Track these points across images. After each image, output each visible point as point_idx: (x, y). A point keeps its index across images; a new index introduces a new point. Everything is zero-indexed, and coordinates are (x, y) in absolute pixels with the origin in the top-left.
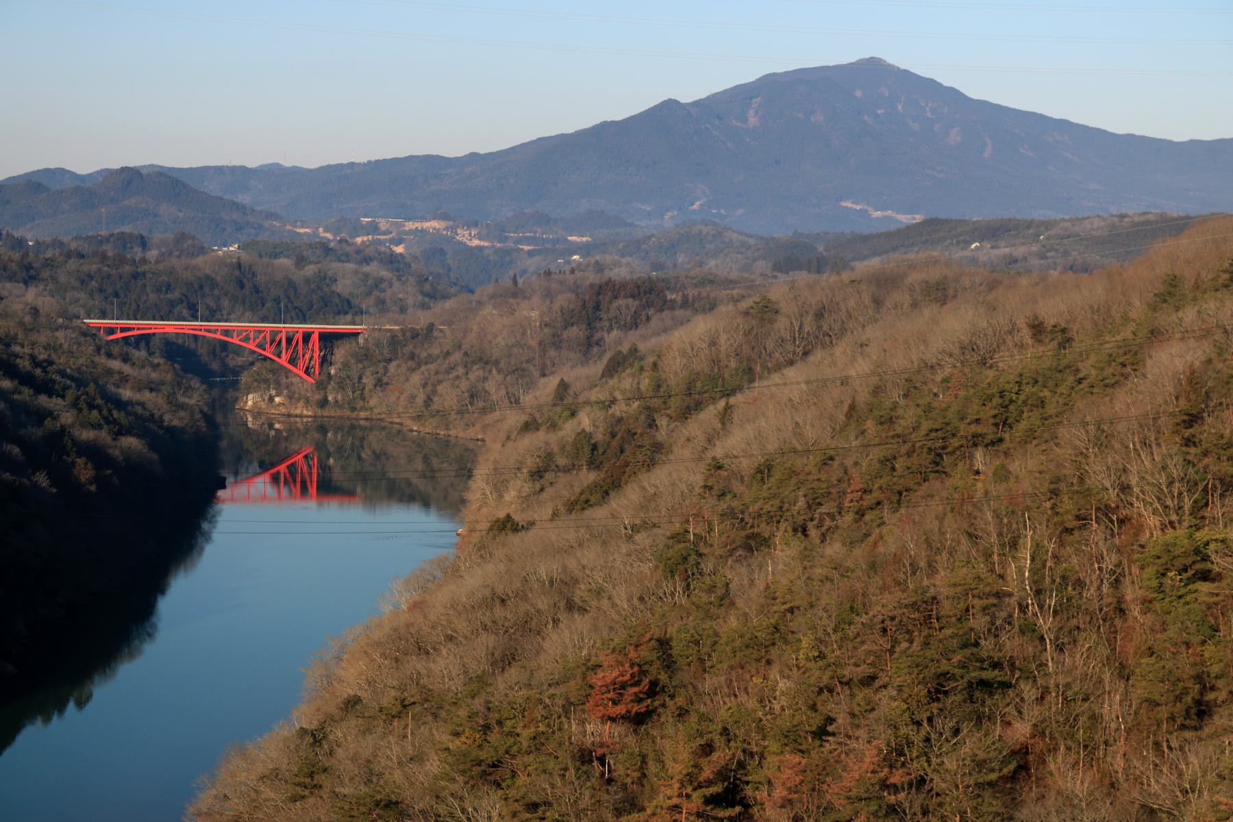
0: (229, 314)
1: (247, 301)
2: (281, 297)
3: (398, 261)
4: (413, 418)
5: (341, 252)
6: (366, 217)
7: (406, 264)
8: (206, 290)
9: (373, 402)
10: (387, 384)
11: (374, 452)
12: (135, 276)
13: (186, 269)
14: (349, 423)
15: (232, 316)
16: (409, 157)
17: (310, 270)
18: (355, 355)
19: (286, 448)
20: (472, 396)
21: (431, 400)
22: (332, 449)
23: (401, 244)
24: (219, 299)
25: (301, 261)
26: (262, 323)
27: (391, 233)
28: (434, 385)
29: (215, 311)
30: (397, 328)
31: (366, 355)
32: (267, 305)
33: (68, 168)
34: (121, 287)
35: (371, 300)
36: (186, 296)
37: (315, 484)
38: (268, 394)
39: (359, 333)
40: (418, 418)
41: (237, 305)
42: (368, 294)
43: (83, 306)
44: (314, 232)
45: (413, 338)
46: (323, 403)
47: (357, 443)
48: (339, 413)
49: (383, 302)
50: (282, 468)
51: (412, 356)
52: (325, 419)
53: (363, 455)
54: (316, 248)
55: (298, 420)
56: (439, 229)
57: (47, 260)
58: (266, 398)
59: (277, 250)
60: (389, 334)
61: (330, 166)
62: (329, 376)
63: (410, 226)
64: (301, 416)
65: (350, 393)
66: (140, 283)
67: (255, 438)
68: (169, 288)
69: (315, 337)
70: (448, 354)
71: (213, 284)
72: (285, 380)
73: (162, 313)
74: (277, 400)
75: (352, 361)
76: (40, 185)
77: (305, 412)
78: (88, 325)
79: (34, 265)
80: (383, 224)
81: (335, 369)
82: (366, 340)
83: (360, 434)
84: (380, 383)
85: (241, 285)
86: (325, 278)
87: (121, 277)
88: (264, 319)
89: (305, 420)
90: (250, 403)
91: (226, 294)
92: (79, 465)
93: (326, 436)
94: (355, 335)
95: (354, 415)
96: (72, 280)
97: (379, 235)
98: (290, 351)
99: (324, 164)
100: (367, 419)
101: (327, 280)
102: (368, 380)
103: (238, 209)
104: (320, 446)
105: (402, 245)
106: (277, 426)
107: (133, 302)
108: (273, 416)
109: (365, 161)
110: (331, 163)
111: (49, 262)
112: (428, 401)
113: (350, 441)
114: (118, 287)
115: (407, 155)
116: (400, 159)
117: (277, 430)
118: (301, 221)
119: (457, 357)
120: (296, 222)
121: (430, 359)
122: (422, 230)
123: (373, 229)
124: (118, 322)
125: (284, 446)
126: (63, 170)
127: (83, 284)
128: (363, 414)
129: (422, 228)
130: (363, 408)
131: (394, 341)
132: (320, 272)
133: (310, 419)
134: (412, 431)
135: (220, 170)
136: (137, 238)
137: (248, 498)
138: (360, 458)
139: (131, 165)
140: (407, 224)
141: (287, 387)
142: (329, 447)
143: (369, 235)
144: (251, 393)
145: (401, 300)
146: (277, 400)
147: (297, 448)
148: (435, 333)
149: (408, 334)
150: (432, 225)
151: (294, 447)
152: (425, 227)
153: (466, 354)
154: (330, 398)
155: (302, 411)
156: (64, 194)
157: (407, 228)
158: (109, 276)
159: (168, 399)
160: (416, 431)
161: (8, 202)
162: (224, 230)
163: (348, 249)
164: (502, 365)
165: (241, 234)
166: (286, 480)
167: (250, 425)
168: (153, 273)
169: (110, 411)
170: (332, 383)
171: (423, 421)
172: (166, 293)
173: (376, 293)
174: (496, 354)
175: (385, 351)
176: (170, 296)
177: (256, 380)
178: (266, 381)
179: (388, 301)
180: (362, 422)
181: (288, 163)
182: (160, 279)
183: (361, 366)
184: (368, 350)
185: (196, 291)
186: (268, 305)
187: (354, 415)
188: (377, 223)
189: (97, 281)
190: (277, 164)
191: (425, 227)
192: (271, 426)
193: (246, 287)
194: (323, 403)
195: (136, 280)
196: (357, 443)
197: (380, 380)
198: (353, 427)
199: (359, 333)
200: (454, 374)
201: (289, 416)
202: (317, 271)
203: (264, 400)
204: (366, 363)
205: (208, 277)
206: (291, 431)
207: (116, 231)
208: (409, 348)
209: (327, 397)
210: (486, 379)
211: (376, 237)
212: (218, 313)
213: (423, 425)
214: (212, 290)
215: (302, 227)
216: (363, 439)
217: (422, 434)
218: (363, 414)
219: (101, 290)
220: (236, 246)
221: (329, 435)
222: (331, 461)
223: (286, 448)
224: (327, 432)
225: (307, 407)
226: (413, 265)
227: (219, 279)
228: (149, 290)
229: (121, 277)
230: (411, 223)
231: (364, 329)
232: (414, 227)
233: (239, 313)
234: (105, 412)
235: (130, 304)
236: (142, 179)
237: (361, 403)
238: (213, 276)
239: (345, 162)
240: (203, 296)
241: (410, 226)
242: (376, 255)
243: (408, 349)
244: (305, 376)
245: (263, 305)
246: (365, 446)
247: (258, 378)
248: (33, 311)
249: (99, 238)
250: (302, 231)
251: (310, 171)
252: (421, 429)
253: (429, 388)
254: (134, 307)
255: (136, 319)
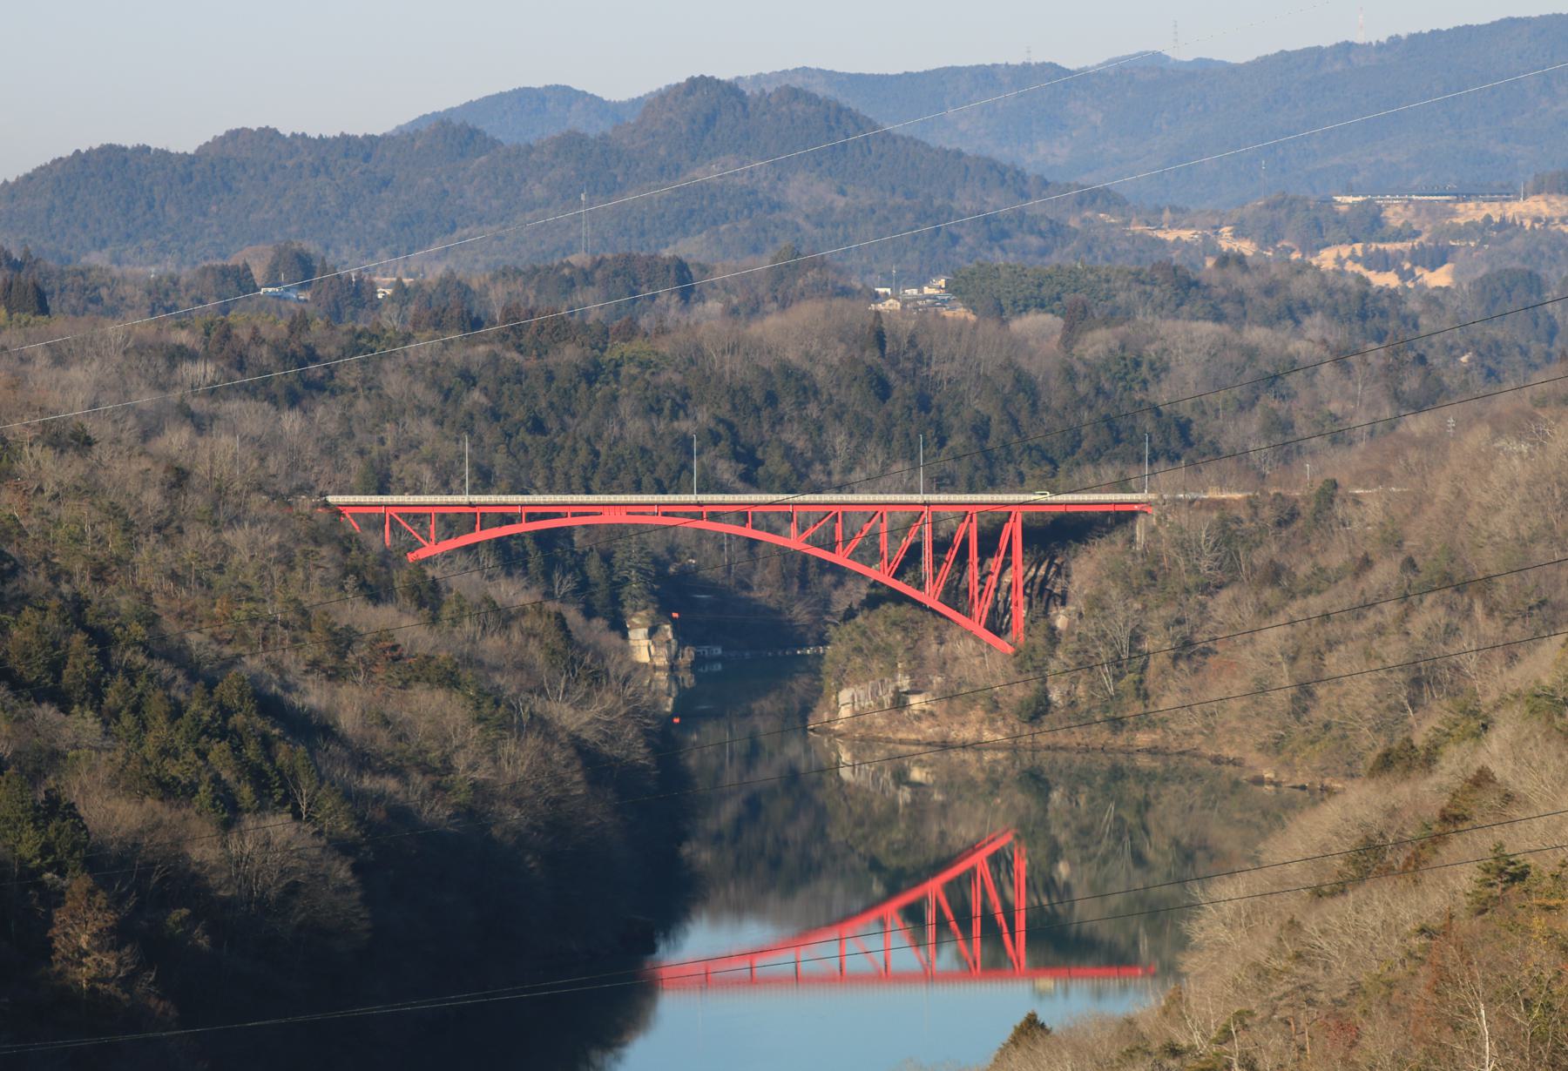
0: (848, 470)
1: (897, 431)
2: (993, 422)
3: (1383, 313)
4: (1262, 748)
5: (1222, 291)
6: (1350, 191)
7: (1404, 319)
8: (787, 405)
9: (1169, 701)
10: (1206, 652)
11: (1176, 842)
12: (591, 374)
13: (732, 350)
14: (1107, 764)
15: (858, 475)
16: (1502, 21)
17: (1097, 343)
18: (1121, 576)
19: (942, 835)
20: (1416, 682)
21: (1311, 695)
22: (1063, 837)
23: (1443, 262)
24: (820, 429)
25: (1078, 319)
26: (939, 491)
27: (1417, 234)
28: (1319, 654)
29: (808, 465)
30: (1237, 496)
31: (1151, 575)
32: (950, 443)
33: (578, 86)
34: (551, 405)
35: (1253, 423)
36: (730, 426)
37: (1021, 937)
38: (891, 688)
39: (1134, 514)
40: (1276, 746)
41: (870, 446)
42: (1244, 407)
43: (430, 461)
44: (1205, 237)
45: (1281, 524)
46: (1038, 710)
47: (1130, 818)
48: (1079, 737)
49: (1286, 426)
50: (933, 889)
51: (1275, 574)
52: (1043, 754)
53: (1150, 854)
54: (1153, 282)
55: (969, 756)
56: (1549, 220)
57: (359, 336)
58: (887, 699)
59: (1045, 291)
60: (1215, 515)
61: (1284, 56)
62: (1053, 636)
63: (1471, 212)
64: (977, 746)
65: (1107, 681)
66: (601, 391)
67: (858, 809)
68: (680, 407)
69: (1014, 529)
70: (1366, 563)
71: (806, 389)
72: (934, 647)
73: (661, 471)
74: (916, 701)
75: (1114, 593)
76: (473, 133)
77: (987, 736)
78: (337, 511)
79: (319, 352)
80: (1395, 213)
81: (1069, 615)
82: (1153, 531)
83: (1138, 792)
84: (1186, 650)
85: (883, 389)
86: (1137, 364)
87: (550, 377)
88: (941, 483)
89: (987, 757)
90: (845, 712)
91: (838, 417)
92: (74, 898)
93: (1046, 800)
94: (1123, 518)
95: (1120, 741)
96: (419, 389)
97: (1383, 240)
98: (946, 570)
99: (1272, 49)
100: (1153, 751)
101: (1144, 369)
102: (1157, 643)
103: (1003, 182)
104: (1032, 830)
105: (1447, 267)
106: (917, 775)
107: (582, 444)
108: (903, 749)
109: (1383, 39)
110: (1289, 49)
111: (364, 341)
112: (1305, 692)
113: (1109, 815)
114: (543, 404)
115: (1497, 16)
116: (1479, 28)
117: (916, 786)
118: (1173, 209)
119: (1385, 572)
120: (1160, 211)
121: (1321, 580)
122: (1503, 224)
123: (1369, 224)
124: (476, 499)
125: (936, 829)
126: (567, 90)
127: (446, 397)
128: (1143, 739)
129: (1503, 219)
130: (1147, 722)
131: (1228, 534)
132: (1123, 348)
133: (1000, 755)
134: (1259, 781)
135: (986, 77)
136: (668, 269)
137: (841, 977)
138: (1139, 859)
139: (725, 74)
140: (1460, 207)
141: (942, 667)
142: (1054, 831)
143: (1356, 241)
144: (848, 685)
145: (1335, 418)
146: (916, 701)
147: (973, 835)
148: (1339, 511)
149: (1267, 513)
150: (1527, 208)
151: (964, 832)
152: (1509, 214)
153: (1410, 564)
154: (1055, 696)
155: (979, 732)
156: (533, 156)
157: (1461, 221)
158: (519, 375)
159: (478, 707)
160: (1271, 782)
161: (386, 183)
162: (955, 239)
163: (1244, 281)
164: (1501, 592)
165: (1003, 249)
166: (941, 924)
167: (845, 773)
168: (641, 364)
169: (266, 743)
170: (1060, 653)
171: (1286, 755)
172: (674, 416)
173: (1269, 401)
174: (1489, 561)
175: (1204, 564)
176: (684, 425)
177: (859, 650)
178: (886, 652)
179: (1299, 421)
180: (1143, 761)
181: (1184, 52)
182: (663, 378)
183: (1137, 606)
184: (1157, 560)
185: (757, 410)
186: (957, 441)
187: (1120, 741)
188: (1380, 208)
189: (485, 390)
190: (1157, 56)
191: (1509, 214)
192: (901, 777)
193: (896, 394)
194: (1038, 710)
195: (590, 383)
196: (1130, 818)
197: (1187, 643)
198: (1117, 774)
199: (1134, 514)
200: (1372, 617)
201: (945, 745)
202: (1115, 344)
203: (881, 704)
204: (1151, 597)
205: (787, 371)
206: (957, 785)
207: (666, 253)
208: (1271, 550)
209: (1046, 692)
210: (1451, 632)
211: (1373, 246)
212: (818, 467)
213: (1287, 764)
214: (801, 405)
215: (1174, 225)
216: (1145, 806)
217: (1285, 791)
218: (1143, 739)
219: (495, 415)
220: (942, 282)
221: (1056, 796)
222: (1063, 869)
223: (943, 835)
224: (1049, 789)
225: (993, 721)
226: (1424, 321)
227: (820, 373)
228: (625, 408)
229: (550, 377)
230: (1471, 205)
231: (1149, 503)
232: (1479, 218)
233: (875, 467)
234: (252, 751)
235: (574, 451)
236: (744, 106)
237: (1138, 707)
238: (806, 366)
239: (1326, 42)
240: (779, 421)
241: (1471, 212)
242: (1322, 296)
243: (1260, 557)
244: (988, 636)
245: (942, 442)
246: (1152, 825)
247: (864, 644)
248: (171, 477)
249: (566, 271)
250: (1171, 236)
251: (1234, 69)
252: (1284, 776)
253: (1305, 663)
254: (583, 456)
255: (589, 492)
